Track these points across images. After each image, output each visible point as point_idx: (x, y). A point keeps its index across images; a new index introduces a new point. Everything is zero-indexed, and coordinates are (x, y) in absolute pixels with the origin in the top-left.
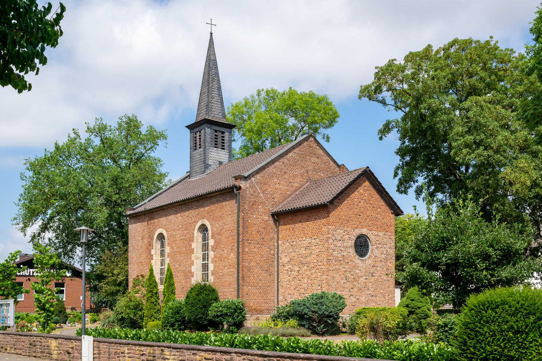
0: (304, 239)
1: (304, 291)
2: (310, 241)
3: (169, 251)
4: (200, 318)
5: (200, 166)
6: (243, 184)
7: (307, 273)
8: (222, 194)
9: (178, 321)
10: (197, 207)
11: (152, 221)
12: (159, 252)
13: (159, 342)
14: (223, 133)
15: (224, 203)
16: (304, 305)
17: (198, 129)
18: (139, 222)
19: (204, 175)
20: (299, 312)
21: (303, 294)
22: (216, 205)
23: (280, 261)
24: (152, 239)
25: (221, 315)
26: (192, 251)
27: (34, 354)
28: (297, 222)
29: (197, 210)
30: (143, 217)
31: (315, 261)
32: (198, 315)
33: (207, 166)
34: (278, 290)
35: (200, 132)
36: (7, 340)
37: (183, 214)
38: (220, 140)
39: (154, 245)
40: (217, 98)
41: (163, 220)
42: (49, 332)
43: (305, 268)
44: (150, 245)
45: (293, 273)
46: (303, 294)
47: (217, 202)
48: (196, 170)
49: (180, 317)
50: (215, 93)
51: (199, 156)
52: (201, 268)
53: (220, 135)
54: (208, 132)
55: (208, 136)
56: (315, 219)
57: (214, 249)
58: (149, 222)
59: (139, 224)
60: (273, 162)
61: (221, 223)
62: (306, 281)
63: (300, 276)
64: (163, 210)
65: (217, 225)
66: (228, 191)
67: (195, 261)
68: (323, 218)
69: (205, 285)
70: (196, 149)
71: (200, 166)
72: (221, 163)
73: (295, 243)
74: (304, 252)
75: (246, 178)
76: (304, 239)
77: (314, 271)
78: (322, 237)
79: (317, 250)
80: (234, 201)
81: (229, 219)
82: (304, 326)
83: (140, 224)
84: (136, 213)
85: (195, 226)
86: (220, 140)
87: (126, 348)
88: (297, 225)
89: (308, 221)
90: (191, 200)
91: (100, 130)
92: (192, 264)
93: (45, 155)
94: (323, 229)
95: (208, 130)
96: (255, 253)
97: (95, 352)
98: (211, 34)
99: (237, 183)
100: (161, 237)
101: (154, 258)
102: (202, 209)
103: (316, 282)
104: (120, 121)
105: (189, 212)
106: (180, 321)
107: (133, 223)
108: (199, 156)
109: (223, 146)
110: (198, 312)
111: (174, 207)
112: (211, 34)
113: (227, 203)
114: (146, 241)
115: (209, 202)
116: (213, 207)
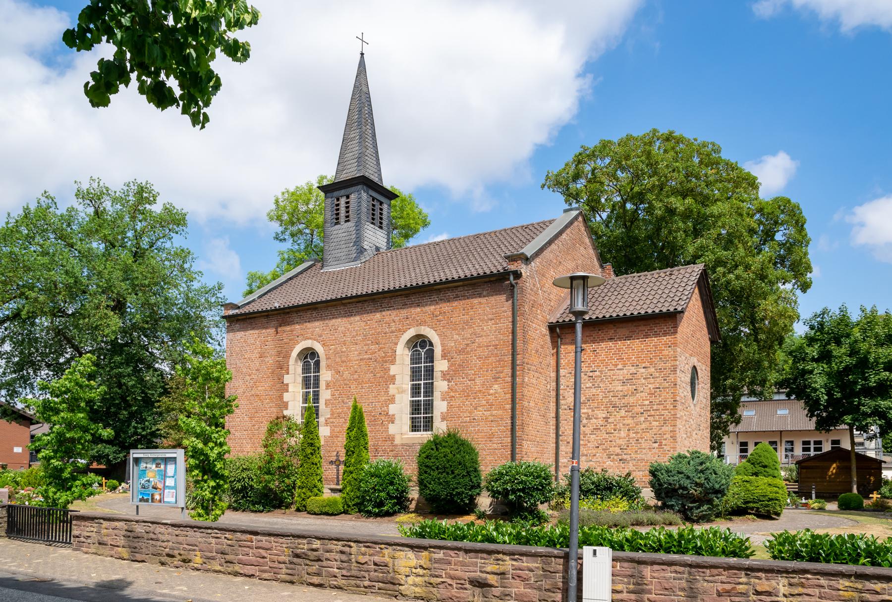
0: (620, 367)
1: (618, 450)
2: (633, 370)
3: (329, 379)
4: (459, 494)
5: (347, 249)
6: (524, 269)
7: (626, 422)
8: (470, 285)
9: (392, 498)
10: (405, 306)
11: (288, 328)
12: (300, 379)
13: (817, 560)
14: (381, 203)
15: (476, 301)
16: (680, 473)
17: (343, 192)
18: (253, 329)
19: (353, 265)
20: (670, 484)
21: (617, 455)
22: (455, 304)
23: (562, 402)
24: (287, 356)
25: (523, 490)
26: (393, 379)
27: (316, 580)
28: (603, 340)
29: (405, 311)
30: (264, 320)
31: (647, 402)
32: (457, 488)
33: (361, 251)
34: (557, 448)
35: (348, 197)
36: (190, 540)
37: (366, 317)
38: (377, 216)
39: (291, 368)
40: (370, 151)
41: (316, 326)
42: (216, 519)
43: (623, 413)
44: (282, 367)
45: (594, 421)
46: (617, 455)
47: (457, 298)
48: (339, 255)
49: (397, 490)
50: (369, 143)
51: (344, 234)
52: (408, 409)
53: (378, 206)
54: (360, 198)
55: (364, 205)
56: (647, 336)
57: (445, 376)
58: (279, 329)
59: (251, 332)
60: (550, 243)
61: (467, 333)
62: (623, 434)
63: (610, 427)
64: (316, 309)
65: (456, 337)
66: (487, 279)
67: (397, 397)
68: (665, 334)
69: (436, 437)
70: (337, 223)
71: (347, 249)
72: (378, 249)
73: (597, 373)
74: (620, 388)
75: (527, 260)
76: (620, 367)
77: (642, 419)
78: (661, 365)
79: (650, 386)
80: (503, 297)
81: (489, 327)
82: (671, 507)
83: (257, 332)
84: (241, 315)
85: (398, 338)
86: (377, 216)
87: (784, 581)
88: (603, 345)
89: (628, 338)
90: (390, 295)
91: (93, 197)
92: (392, 400)
93: (7, 223)
94: (665, 353)
95: (364, 195)
96: (536, 385)
97: (619, 587)
98: (362, 54)
99: (512, 267)
100: (309, 355)
101: (290, 389)
102: (418, 309)
103: (648, 436)
104: (126, 188)
105: (384, 313)
106: (396, 498)
107: (238, 331)
108: (344, 234)
109: (381, 223)
110: (459, 483)
111: (344, 305)
112: (362, 54)
113: (483, 300)
114: (270, 360)
115: (434, 297)
116: (445, 307)
